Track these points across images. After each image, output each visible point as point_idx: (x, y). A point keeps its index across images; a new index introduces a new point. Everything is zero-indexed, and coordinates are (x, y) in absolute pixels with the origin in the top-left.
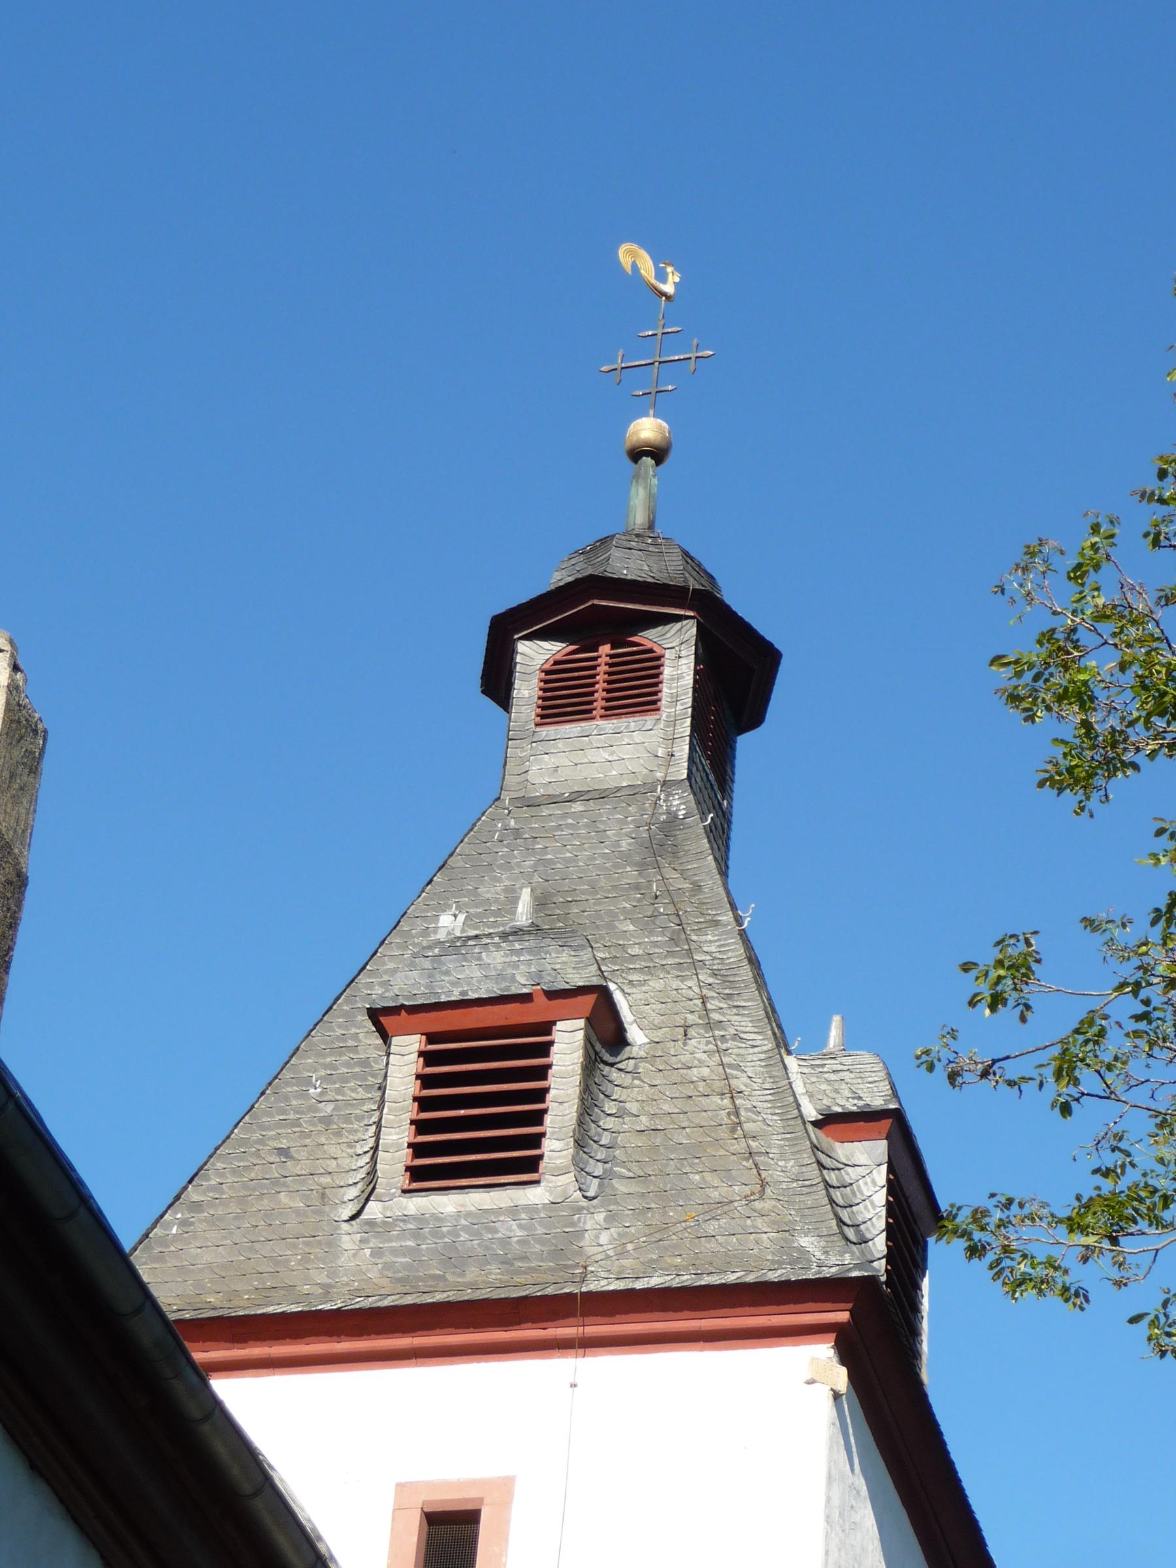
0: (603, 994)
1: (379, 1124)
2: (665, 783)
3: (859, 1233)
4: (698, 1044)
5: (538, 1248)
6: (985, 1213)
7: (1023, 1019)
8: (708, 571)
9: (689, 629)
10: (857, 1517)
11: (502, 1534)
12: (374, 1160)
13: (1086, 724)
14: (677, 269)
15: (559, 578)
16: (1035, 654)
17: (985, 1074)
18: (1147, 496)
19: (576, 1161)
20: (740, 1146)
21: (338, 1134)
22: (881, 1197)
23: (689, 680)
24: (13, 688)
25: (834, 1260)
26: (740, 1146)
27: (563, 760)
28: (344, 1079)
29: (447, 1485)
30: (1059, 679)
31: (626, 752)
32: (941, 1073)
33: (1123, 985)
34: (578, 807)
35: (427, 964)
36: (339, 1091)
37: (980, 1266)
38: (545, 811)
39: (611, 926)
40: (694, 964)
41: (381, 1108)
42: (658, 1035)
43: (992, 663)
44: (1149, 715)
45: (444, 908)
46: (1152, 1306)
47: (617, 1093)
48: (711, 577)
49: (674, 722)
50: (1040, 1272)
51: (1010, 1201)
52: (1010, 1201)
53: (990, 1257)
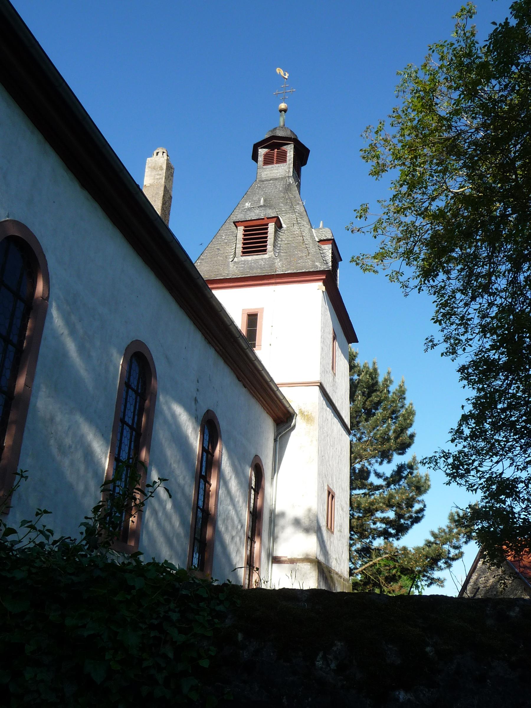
0: (278, 218)
1: (236, 243)
2: (288, 177)
3: (326, 262)
4: (296, 227)
5: (267, 266)
6: (359, 257)
7: (365, 220)
8: (295, 133)
9: (292, 146)
10: (327, 313)
11: (262, 318)
12: (235, 250)
13: (378, 162)
14: (288, 73)
15: (267, 136)
16: (368, 149)
17: (358, 231)
18: (390, 116)
19: (273, 250)
20: (304, 246)
21: (228, 246)
22: (330, 255)
23: (292, 156)
24: (167, 160)
25: (322, 267)
26: (304, 246)
27: (268, 173)
28: (229, 235)
29: (251, 309)
30: (373, 153)
31: (280, 171)
32: (350, 231)
33: (385, 213)
34: (271, 182)
35: (244, 213)
36: (228, 237)
37: (359, 267)
38: (265, 183)
39: (278, 205)
40: (295, 212)
41: (236, 240)
42: (288, 226)
43: (360, 151)
44: (394, 159)
45: (247, 202)
46: (390, 273)
47: (281, 237)
48: (296, 136)
49: (289, 164)
50: (370, 268)
51: (364, 255)
52: (364, 255)
53: (360, 265)
